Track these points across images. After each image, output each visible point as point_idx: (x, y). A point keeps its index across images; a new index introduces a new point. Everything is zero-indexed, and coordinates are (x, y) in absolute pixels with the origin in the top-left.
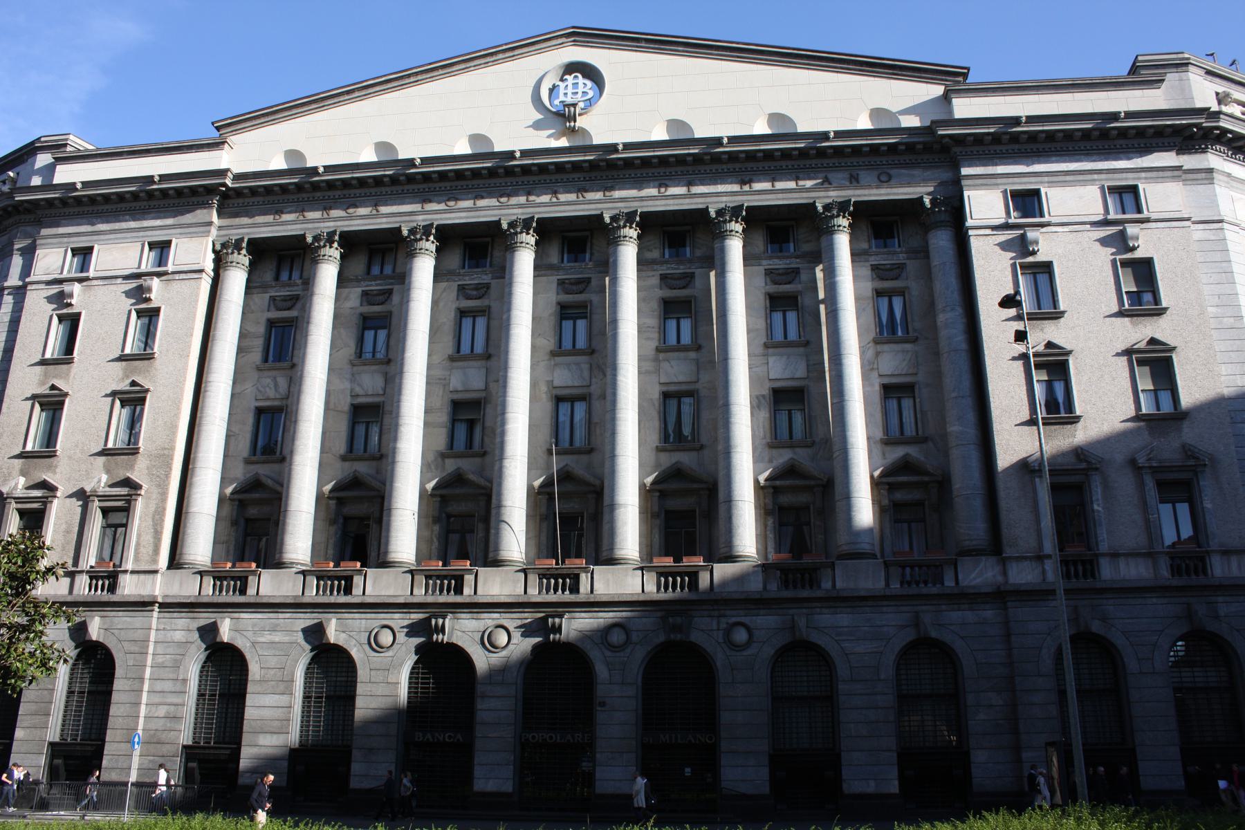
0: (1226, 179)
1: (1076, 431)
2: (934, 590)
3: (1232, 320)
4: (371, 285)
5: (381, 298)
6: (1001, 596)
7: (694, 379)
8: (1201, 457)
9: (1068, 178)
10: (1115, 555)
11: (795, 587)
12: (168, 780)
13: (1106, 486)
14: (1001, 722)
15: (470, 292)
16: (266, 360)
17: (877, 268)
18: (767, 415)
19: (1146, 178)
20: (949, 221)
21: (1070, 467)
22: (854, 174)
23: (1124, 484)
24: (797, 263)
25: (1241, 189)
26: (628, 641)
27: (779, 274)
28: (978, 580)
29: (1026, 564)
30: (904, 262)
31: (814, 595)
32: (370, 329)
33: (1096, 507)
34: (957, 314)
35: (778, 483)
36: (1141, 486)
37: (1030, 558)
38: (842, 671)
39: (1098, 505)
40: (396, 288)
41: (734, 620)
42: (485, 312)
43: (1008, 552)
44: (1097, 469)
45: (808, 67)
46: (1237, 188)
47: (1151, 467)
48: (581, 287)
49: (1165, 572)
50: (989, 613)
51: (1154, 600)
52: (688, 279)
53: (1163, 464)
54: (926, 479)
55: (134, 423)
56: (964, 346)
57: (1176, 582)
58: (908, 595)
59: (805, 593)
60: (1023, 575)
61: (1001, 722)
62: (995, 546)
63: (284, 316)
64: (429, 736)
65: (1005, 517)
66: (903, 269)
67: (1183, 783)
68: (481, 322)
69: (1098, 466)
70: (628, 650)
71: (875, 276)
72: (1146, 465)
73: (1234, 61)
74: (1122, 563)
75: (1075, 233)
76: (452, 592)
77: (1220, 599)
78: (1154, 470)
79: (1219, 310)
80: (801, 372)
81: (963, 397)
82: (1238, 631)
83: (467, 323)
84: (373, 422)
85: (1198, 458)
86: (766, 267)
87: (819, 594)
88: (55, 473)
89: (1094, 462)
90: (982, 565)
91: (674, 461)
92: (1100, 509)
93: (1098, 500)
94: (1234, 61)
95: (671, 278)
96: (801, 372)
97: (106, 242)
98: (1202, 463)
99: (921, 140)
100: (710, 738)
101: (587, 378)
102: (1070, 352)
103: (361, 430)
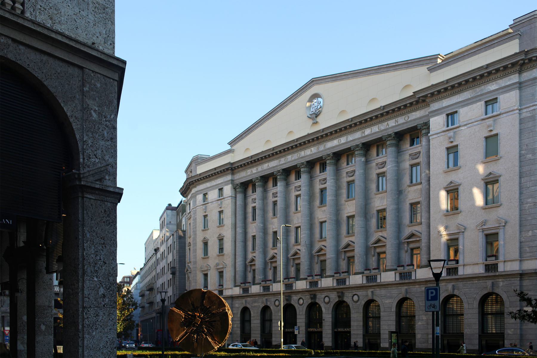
2: (375, 284)
11: (405, 279)
12: (114, 324)
19: (502, 92)
26: (329, 301)
30: (420, 150)
38: (382, 309)
41: (355, 293)
51: (476, 281)
58: (402, 283)
59: (406, 281)
64: (345, 329)
65: (236, 278)
67: (478, 347)
68: (419, 167)
70: (329, 304)
75: (470, 128)
77: (500, 280)
82: (505, 292)
83: (414, 169)
87: (411, 281)
91: (410, 231)
97: (211, 190)
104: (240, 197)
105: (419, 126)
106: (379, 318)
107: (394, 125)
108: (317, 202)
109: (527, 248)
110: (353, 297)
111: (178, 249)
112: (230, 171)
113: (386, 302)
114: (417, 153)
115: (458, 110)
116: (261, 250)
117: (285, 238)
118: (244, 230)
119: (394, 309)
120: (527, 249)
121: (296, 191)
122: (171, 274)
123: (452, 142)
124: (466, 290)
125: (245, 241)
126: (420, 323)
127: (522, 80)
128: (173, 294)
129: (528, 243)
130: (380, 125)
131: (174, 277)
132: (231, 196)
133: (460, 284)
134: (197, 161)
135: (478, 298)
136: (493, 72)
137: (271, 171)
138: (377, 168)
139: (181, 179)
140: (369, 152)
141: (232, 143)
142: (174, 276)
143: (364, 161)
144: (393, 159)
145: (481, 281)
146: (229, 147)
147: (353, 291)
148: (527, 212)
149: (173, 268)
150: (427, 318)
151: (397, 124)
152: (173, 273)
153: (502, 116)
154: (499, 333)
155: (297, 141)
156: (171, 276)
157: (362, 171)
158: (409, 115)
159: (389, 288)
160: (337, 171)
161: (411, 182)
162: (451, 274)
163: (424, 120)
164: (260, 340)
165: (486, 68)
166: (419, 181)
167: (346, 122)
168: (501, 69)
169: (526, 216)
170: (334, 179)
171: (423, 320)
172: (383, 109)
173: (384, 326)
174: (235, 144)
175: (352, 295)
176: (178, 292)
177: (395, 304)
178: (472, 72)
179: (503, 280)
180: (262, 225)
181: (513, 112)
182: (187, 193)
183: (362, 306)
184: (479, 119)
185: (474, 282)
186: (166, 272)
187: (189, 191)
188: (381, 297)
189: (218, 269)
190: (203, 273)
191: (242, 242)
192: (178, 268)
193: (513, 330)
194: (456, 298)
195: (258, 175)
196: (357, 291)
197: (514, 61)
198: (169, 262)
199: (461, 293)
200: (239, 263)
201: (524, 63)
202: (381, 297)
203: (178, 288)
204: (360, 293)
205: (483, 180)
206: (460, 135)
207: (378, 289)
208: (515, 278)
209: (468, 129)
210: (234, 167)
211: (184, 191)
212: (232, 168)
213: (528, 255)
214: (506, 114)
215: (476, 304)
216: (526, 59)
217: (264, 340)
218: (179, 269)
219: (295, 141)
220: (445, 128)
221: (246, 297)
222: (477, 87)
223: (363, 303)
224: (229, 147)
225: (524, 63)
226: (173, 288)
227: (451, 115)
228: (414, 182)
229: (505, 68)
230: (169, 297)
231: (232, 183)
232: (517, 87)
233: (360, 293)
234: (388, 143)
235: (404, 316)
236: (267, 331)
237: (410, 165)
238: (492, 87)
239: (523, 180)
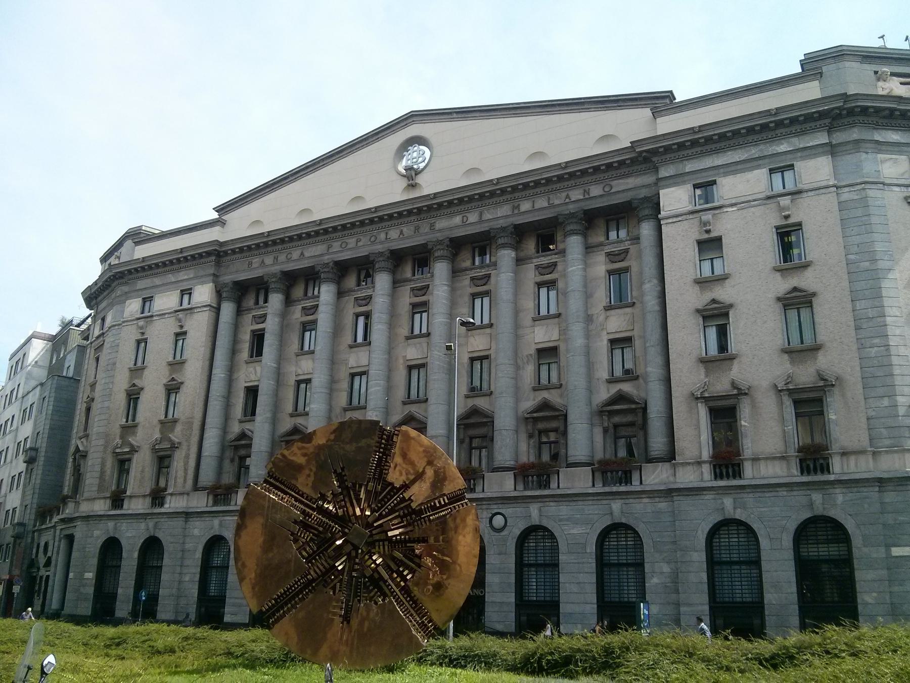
0: (872, 145)
1: (732, 365)
3: (867, 264)
4: (307, 303)
5: (364, 302)
6: (669, 493)
7: (631, 328)
8: (829, 379)
9: (739, 167)
10: (755, 460)
13: (754, 406)
14: (668, 584)
15: (360, 302)
16: (252, 356)
17: (305, 309)
18: (533, 368)
20: (651, 215)
21: (724, 394)
22: (587, 189)
23: (768, 404)
24: (556, 258)
25: (891, 151)
27: (544, 268)
28: (657, 481)
29: (689, 468)
30: (628, 247)
31: (630, 490)
32: (308, 331)
33: (743, 423)
34: (652, 284)
35: (535, 415)
36: (781, 403)
37: (692, 464)
38: (563, 547)
39: (745, 421)
40: (493, 272)
41: (496, 511)
42: (487, 293)
43: (679, 459)
44: (746, 394)
45: (560, 112)
46: (887, 150)
47: (788, 390)
48: (551, 269)
49: (795, 471)
50: (663, 505)
52: (487, 278)
53: (798, 387)
54: (633, 406)
55: (722, 333)
56: (657, 308)
57: (805, 479)
59: (623, 488)
60: (687, 477)
61: (668, 584)
62: (670, 456)
63: (421, 300)
66: (628, 252)
68: (486, 300)
69: (746, 391)
71: (608, 260)
72: (785, 388)
73: (907, 37)
74: (762, 464)
76: (819, 471)
77: (838, 491)
78: (791, 392)
79: (858, 257)
80: (555, 336)
81: (652, 346)
82: (850, 515)
83: (478, 302)
84: (552, 363)
85: (826, 380)
86: (536, 264)
88: (136, 436)
89: (743, 388)
90: (659, 468)
92: (746, 424)
93: (745, 417)
94: (907, 37)
95: (477, 279)
96: (555, 336)
97: (726, 174)
98: (830, 383)
99: (689, 138)
100: (482, 592)
101: (425, 350)
102: (814, 294)
103: (544, 369)
104: (228, 309)
105: (431, 243)
106: (555, 565)
107: (582, 197)
108: (245, 354)
109: (882, 430)
110: (491, 519)
111: (50, 412)
112: (214, 258)
113: (572, 531)
114: (621, 252)
115: (795, 163)
116: (269, 415)
117: (328, 392)
118: (228, 373)
119: (592, 548)
120: (884, 431)
121: (356, 305)
122: (25, 462)
123: (708, 232)
124: (763, 509)
125: (228, 398)
126: (655, 580)
127: (834, 142)
128: (21, 505)
129: (883, 420)
130: (551, 196)
131: (29, 471)
132: (209, 305)
133: (749, 498)
134: (136, 236)
135: (792, 526)
136: (590, 171)
137: (352, 255)
138: (537, 273)
139: (93, 272)
140: (400, 269)
141: (223, 209)
142: (30, 469)
143: (514, 257)
144: (580, 256)
145: (795, 493)
146: (215, 215)
147: (493, 506)
148: (875, 362)
149: (34, 449)
150: (671, 569)
151: (587, 196)
152: (30, 461)
153: (805, 195)
154: (542, 601)
155: (375, 212)
156: (22, 467)
157: (511, 274)
158: (614, 183)
159: (580, 503)
160: (289, 301)
161: (302, 349)
162: (812, 472)
163: (643, 193)
164: (707, 612)
165: (566, 167)
166: (424, 331)
167: (487, 184)
168: (589, 171)
169: (872, 369)
170: (448, 285)
171: (662, 573)
172: (566, 167)
173: (567, 585)
174: (227, 212)
175: (491, 515)
176: (35, 501)
177: (595, 538)
178: (576, 163)
179: (844, 490)
180: (275, 365)
181: (826, 189)
182: (100, 298)
183: (515, 540)
184: (761, 196)
185: (780, 494)
186: (9, 459)
187: (107, 292)
188: (560, 520)
189: (118, 454)
190: (119, 457)
191: (223, 397)
192: (43, 449)
193: (875, 594)
194: (542, 534)
195: (424, 240)
196: (500, 506)
197: (826, 108)
198: (21, 438)
199: (752, 516)
200: (212, 440)
201: (840, 114)
202: (560, 520)
203: (37, 491)
204: (510, 510)
205: (779, 299)
206: (725, 221)
207: (552, 504)
208: (869, 486)
209: (741, 211)
210: (224, 251)
211: (92, 297)
212: (219, 252)
213: (887, 442)
214: (813, 192)
215: (787, 541)
216: (845, 109)
217: (203, 609)
218: (46, 452)
219: (265, 235)
220: (691, 208)
221: (221, 515)
222: (687, 160)
223: (517, 532)
224: (215, 215)
225: (839, 116)
226: (24, 492)
227: (706, 187)
228: (417, 331)
229: (201, 255)
230: (8, 511)
231: (214, 282)
232: (827, 151)
233: (508, 511)
234: (500, 241)
235: (530, 565)
236: (213, 590)
237: (410, 304)
238: (141, 284)
239: (858, 305)
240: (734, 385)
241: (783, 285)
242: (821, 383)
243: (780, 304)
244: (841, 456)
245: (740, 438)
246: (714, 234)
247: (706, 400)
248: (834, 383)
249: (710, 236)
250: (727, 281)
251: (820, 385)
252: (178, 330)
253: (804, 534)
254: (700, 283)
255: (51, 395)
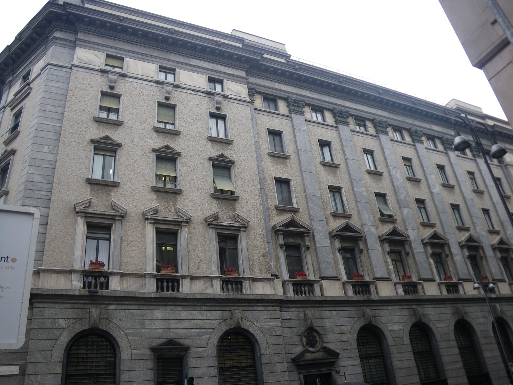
49: (400, 290)
57: (409, 297)
115: (125, 57)
153: (127, 79)
240: (113, 207)
241: (158, 142)
242: (113, 213)
243: (154, 156)
244: (121, 277)
245: (219, 258)
246: (172, 102)
247: (86, 215)
248: (246, 226)
249: (167, 102)
250: (120, 126)
251: (112, 214)
252: (106, 89)
253: (76, 344)
254: (213, 141)
255: (123, 131)
